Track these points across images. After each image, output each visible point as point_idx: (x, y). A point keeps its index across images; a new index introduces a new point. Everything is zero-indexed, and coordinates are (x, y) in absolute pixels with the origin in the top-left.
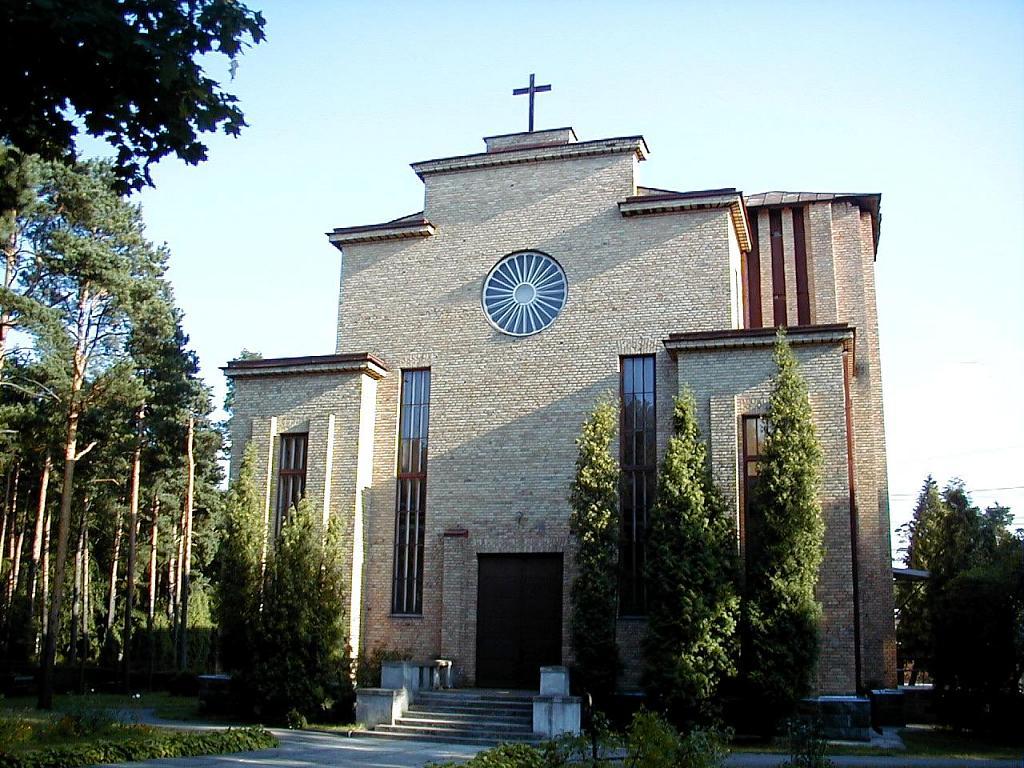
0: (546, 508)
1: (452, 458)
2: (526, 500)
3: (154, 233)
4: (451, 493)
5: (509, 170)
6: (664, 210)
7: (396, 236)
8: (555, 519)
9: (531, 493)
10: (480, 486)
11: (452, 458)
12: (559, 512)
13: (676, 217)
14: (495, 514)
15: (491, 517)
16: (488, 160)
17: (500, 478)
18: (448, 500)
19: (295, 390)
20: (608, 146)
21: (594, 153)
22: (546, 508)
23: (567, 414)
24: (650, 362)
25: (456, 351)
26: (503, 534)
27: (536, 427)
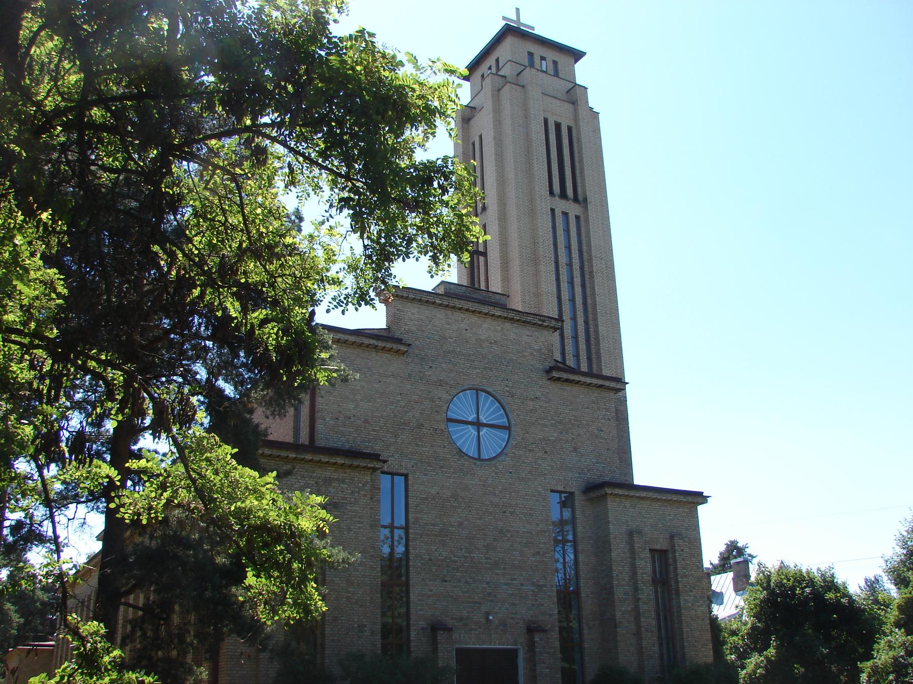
0: (507, 609)
1: (430, 560)
2: (491, 601)
3: (393, 271)
4: (431, 591)
5: (462, 315)
6: (578, 382)
7: (376, 347)
8: (513, 618)
9: (495, 596)
10: (455, 587)
11: (430, 560)
12: (516, 613)
13: (582, 389)
14: (468, 612)
15: (465, 614)
16: (431, 299)
17: (470, 580)
18: (429, 597)
19: (303, 477)
20: (540, 320)
21: (528, 323)
22: (507, 609)
23: (518, 532)
24: (399, 480)
25: (429, 464)
26: (475, 630)
27: (495, 540)
